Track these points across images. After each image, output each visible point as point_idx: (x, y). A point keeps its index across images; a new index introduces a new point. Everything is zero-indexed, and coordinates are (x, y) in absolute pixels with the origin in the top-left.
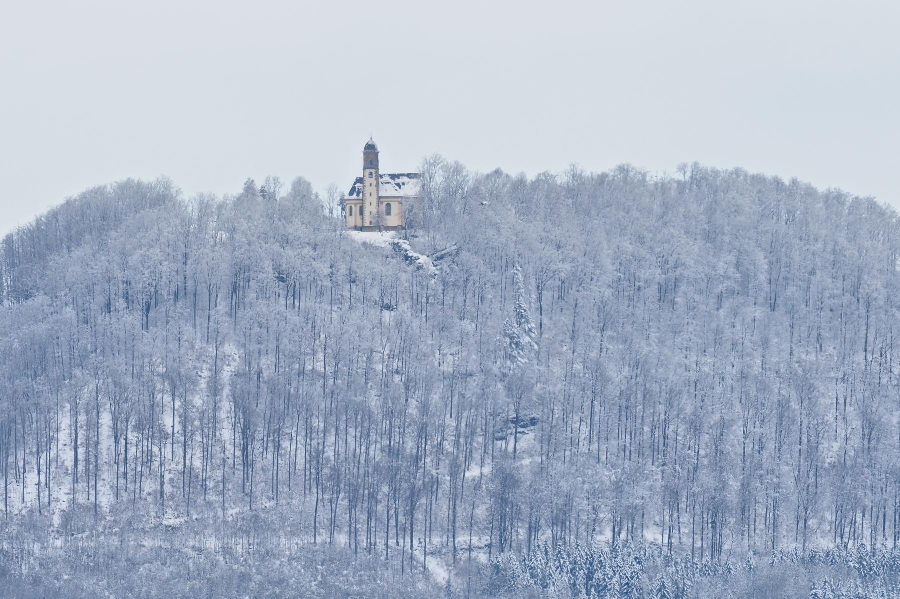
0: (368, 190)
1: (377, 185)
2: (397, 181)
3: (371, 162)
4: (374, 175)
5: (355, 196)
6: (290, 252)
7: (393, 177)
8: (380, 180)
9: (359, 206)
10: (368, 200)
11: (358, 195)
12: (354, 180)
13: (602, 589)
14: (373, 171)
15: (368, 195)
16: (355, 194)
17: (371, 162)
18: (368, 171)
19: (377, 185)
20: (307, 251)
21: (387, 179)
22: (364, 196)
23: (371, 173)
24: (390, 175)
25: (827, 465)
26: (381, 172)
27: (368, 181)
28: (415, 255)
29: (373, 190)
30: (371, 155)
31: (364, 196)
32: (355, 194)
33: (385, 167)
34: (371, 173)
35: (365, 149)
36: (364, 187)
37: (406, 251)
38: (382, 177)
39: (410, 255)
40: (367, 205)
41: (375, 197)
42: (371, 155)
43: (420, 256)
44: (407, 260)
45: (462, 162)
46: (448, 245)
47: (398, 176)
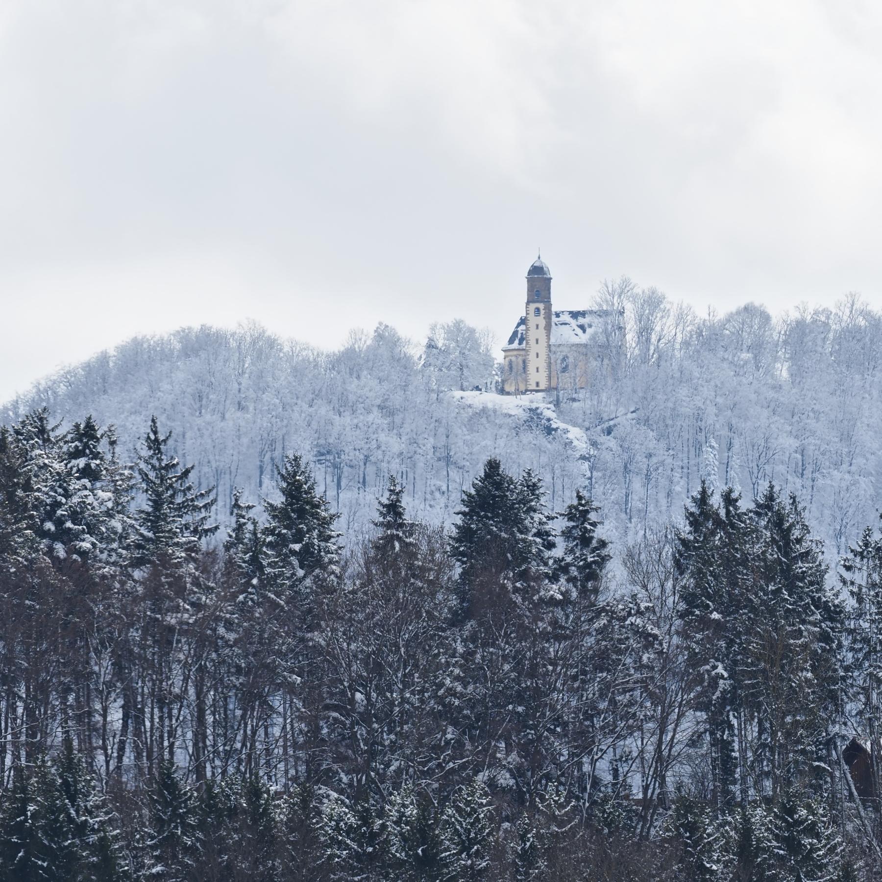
0: (532, 335)
1: (548, 327)
2: (581, 320)
3: (538, 293)
4: (542, 312)
5: (515, 345)
6: (347, 419)
7: (575, 315)
8: (554, 319)
9: (520, 359)
10: (534, 349)
11: (520, 344)
12: (518, 320)
13: (810, 863)
14: (541, 306)
15: (532, 342)
16: (517, 341)
17: (538, 293)
18: (533, 306)
19: (548, 327)
20: (375, 417)
21: (566, 318)
22: (527, 343)
23: (538, 309)
24: (570, 313)
25: (536, 598)
26: (554, 309)
27: (533, 320)
28: (562, 426)
29: (541, 333)
30: (539, 283)
31: (527, 343)
32: (517, 341)
33: (562, 299)
34: (538, 309)
35: (530, 273)
36: (527, 330)
37: (549, 420)
38: (558, 315)
39: (554, 426)
40: (532, 357)
41: (542, 348)
42: (539, 283)
43: (570, 428)
44: (549, 433)
45: (661, 289)
46: (622, 410)
47: (583, 314)
